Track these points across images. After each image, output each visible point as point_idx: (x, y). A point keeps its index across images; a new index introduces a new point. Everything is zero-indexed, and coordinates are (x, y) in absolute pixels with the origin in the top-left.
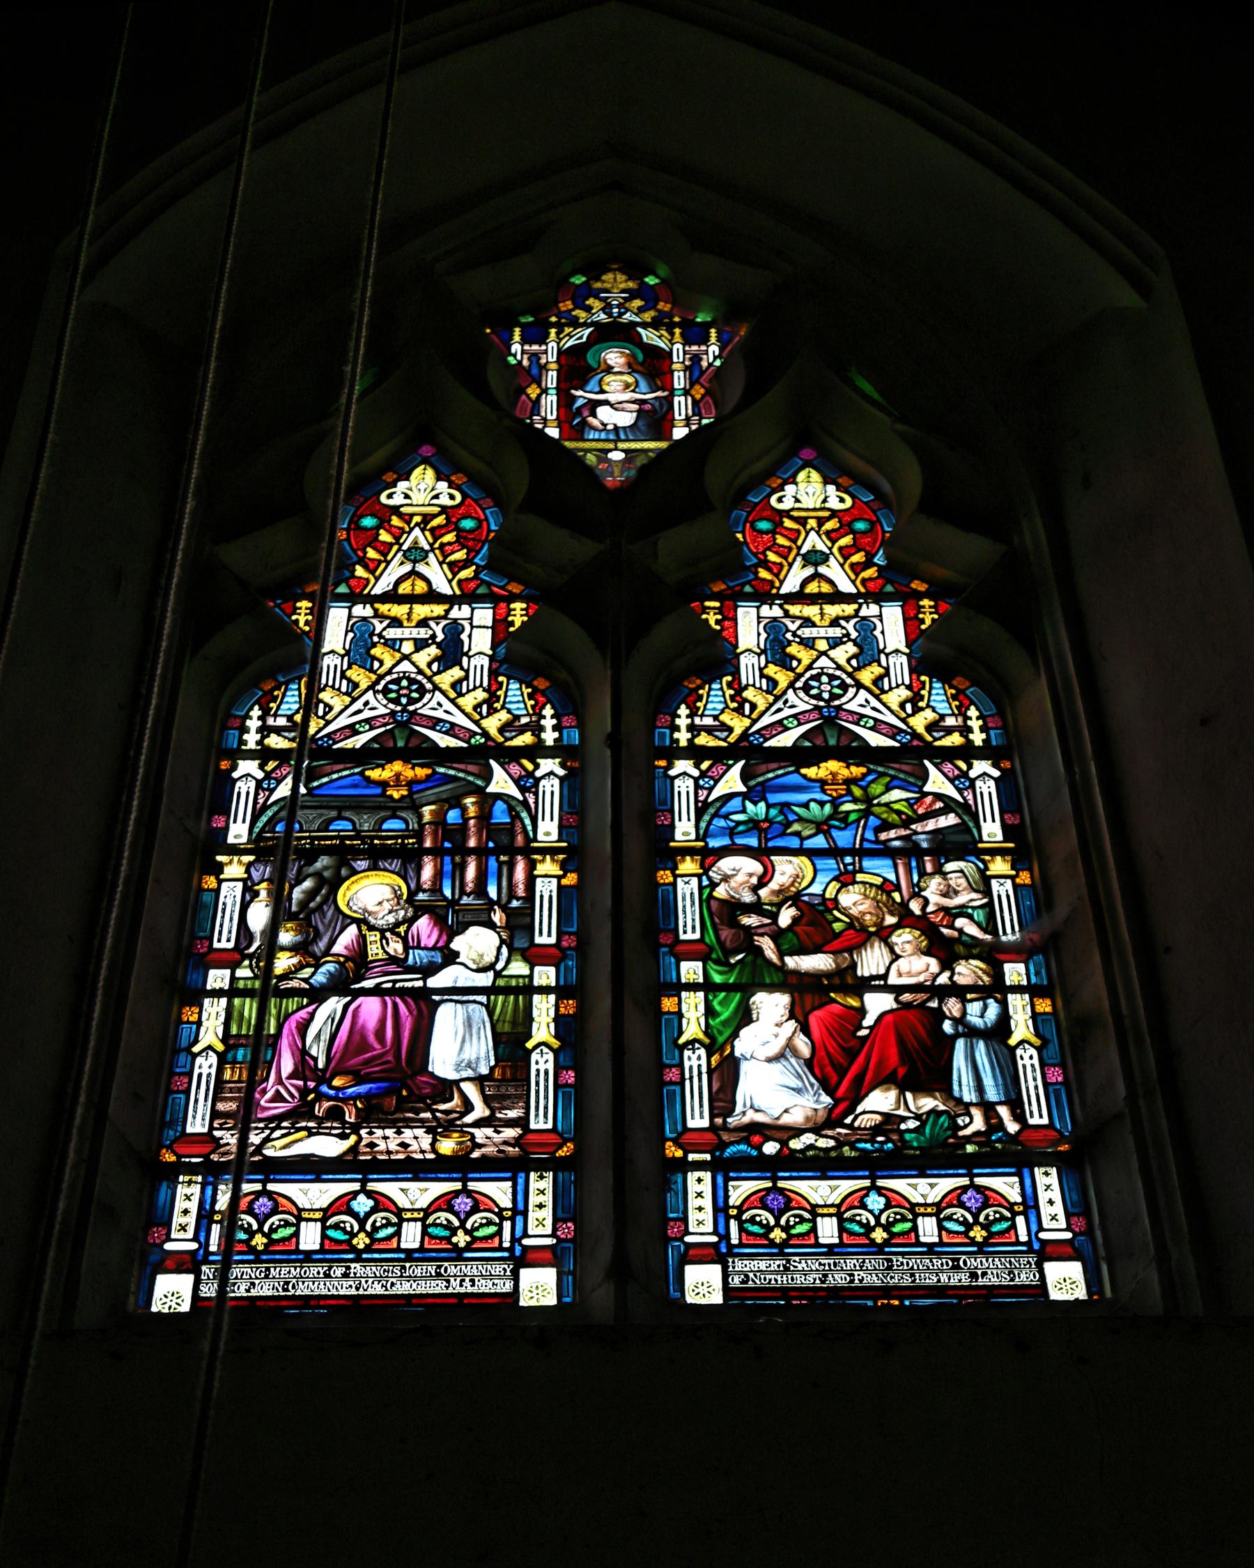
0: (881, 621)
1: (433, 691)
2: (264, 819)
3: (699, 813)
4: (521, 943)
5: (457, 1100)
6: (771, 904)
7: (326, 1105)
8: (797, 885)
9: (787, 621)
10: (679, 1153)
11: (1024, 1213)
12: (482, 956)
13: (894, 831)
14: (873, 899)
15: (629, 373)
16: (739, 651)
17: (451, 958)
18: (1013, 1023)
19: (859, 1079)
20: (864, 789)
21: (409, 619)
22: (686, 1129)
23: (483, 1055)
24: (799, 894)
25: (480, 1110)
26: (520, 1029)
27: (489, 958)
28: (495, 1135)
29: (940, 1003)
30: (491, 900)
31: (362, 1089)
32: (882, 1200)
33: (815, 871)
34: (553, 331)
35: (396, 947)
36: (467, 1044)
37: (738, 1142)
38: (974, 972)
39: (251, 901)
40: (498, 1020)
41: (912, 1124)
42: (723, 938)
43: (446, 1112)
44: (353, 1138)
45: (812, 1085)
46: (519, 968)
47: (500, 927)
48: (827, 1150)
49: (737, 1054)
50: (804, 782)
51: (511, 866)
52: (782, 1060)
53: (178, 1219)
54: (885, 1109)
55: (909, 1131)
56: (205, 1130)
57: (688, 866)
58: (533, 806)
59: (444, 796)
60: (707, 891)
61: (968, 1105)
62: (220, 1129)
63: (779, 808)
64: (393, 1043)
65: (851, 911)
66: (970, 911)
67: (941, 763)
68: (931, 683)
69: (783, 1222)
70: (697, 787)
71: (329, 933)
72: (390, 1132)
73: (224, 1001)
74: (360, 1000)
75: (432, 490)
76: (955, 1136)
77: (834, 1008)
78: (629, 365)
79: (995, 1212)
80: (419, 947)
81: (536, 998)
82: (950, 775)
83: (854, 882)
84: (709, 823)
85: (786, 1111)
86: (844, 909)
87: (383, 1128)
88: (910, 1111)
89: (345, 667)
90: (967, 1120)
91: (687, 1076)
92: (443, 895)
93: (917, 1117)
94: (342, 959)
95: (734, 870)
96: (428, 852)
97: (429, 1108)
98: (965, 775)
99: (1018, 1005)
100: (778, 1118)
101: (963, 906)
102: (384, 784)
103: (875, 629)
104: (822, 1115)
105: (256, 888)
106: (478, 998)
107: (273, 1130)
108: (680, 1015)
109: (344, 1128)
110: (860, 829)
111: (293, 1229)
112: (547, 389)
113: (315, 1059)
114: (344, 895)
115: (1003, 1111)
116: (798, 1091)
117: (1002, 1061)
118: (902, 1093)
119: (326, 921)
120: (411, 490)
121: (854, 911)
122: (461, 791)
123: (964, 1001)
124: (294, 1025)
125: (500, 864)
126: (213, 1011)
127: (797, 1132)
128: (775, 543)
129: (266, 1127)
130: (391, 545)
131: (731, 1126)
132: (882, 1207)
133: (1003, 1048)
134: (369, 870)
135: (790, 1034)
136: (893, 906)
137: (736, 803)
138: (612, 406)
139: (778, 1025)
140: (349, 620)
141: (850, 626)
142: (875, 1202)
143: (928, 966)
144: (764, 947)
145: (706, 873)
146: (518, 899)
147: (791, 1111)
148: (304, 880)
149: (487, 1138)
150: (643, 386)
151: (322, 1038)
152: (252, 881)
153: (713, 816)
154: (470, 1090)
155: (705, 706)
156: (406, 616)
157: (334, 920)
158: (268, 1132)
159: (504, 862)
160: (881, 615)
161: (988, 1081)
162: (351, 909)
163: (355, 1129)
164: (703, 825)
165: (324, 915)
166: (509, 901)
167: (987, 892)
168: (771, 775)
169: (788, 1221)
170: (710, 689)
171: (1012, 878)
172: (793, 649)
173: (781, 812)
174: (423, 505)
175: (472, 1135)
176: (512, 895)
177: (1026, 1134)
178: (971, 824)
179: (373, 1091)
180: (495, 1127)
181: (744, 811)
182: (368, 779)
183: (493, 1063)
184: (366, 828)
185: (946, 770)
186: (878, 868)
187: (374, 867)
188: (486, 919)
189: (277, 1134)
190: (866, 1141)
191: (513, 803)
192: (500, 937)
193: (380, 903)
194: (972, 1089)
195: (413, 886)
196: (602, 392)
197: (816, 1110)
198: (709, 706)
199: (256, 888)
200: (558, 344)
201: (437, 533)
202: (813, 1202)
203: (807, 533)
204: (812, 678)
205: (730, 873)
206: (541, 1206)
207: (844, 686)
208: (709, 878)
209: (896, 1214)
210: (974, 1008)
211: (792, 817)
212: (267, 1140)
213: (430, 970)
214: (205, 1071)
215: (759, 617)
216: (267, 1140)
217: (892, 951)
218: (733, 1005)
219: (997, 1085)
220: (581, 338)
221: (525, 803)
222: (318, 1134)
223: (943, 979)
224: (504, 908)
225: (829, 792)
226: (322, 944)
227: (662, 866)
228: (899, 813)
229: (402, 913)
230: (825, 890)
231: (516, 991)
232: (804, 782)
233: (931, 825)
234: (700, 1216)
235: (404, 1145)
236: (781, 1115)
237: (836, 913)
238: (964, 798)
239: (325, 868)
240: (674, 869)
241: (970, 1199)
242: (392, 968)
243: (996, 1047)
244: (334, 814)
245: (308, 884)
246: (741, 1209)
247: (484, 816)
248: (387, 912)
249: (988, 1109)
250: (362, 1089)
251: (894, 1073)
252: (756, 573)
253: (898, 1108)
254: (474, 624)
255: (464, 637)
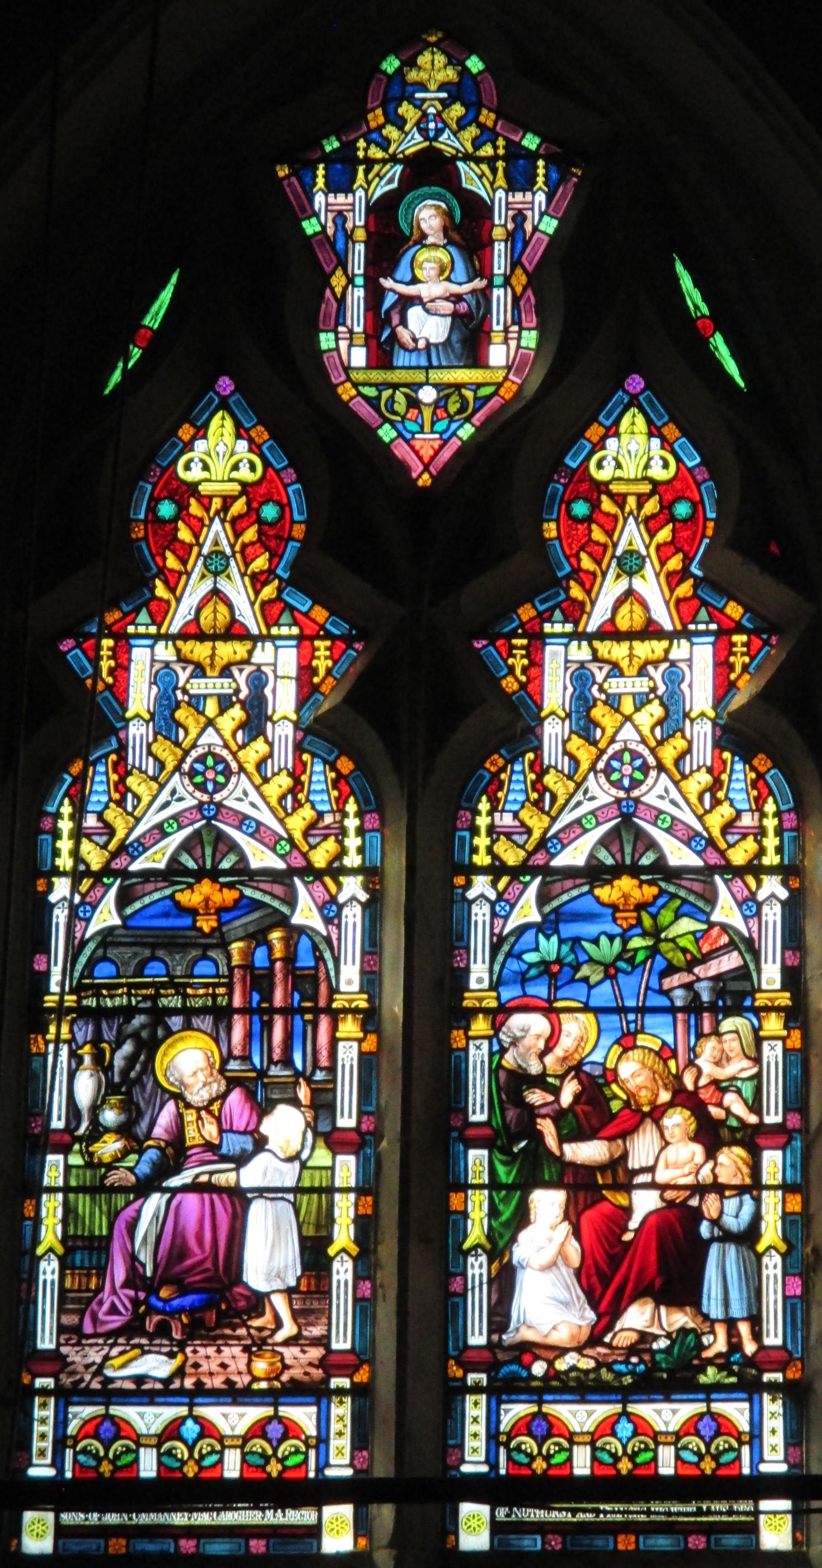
0: (690, 667)
1: (239, 773)
2: (83, 960)
3: (495, 949)
4: (325, 1127)
5: (268, 1315)
6: (555, 1076)
7: (156, 1318)
8: (580, 1050)
9: (593, 667)
10: (459, 1373)
11: (750, 1443)
12: (288, 1142)
13: (676, 976)
14: (651, 1069)
15: (444, 247)
16: (543, 714)
17: (260, 1144)
18: (763, 1225)
19: (621, 1289)
20: (654, 917)
21: (212, 665)
22: (467, 1347)
23: (290, 1263)
24: (581, 1063)
25: (289, 1329)
26: (323, 1233)
27: (295, 1146)
28: (300, 1355)
29: (701, 1200)
30: (296, 1069)
31: (189, 1300)
32: (630, 1427)
33: (599, 1031)
34: (361, 169)
35: (211, 1130)
36: (276, 1253)
37: (510, 1362)
38: (735, 1163)
39: (77, 1069)
40: (303, 1222)
41: (663, 1343)
42: (508, 1119)
43: (260, 1329)
44: (180, 1358)
45: (578, 1298)
46: (322, 1157)
47: (305, 1106)
48: (587, 1372)
49: (515, 1261)
50: (597, 908)
51: (315, 1025)
52: (554, 1268)
53: (36, 1444)
54: (639, 1327)
55: (660, 1351)
56: (53, 1346)
57: (480, 1026)
58: (335, 943)
59: (251, 929)
60: (496, 1058)
61: (713, 1322)
62: (66, 1344)
63: (570, 943)
64: (211, 1247)
65: (628, 1085)
66: (739, 1083)
67: (731, 880)
68: (733, 763)
69: (544, 1451)
70: (494, 915)
71: (150, 1112)
72: (211, 1351)
73: (60, 1196)
74: (179, 1197)
75: (232, 455)
76: (698, 1357)
77: (603, 1207)
78: (445, 230)
79: (725, 1442)
80: (231, 1131)
81: (337, 1197)
82: (739, 896)
83: (634, 1047)
84: (503, 966)
85: (554, 1328)
86: (623, 1081)
87: (205, 1346)
88: (663, 1329)
89: (151, 739)
90: (711, 1338)
91: (470, 1286)
92: (252, 1064)
93: (668, 1336)
94: (163, 1144)
95: (523, 1030)
96: (239, 1011)
97: (244, 1324)
98: (753, 895)
99: (772, 1202)
100: (546, 1336)
101: (734, 1078)
102: (193, 912)
103: (683, 680)
104: (585, 1335)
105: (80, 1052)
106: (286, 1196)
107: (112, 1346)
108: (465, 1214)
109: (171, 1345)
110: (646, 973)
111: (133, 1456)
112: (354, 275)
113: (144, 1266)
114: (162, 1063)
115: (744, 1329)
116: (566, 1304)
117: (749, 1270)
118: (657, 1307)
119: (146, 1096)
120: (210, 456)
121: (631, 1085)
122: (267, 922)
123: (722, 1197)
124: (123, 1226)
125: (305, 1023)
126: (51, 1205)
127: (562, 1351)
128: (590, 540)
129: (105, 1344)
130: (191, 546)
131: (506, 1344)
132: (629, 1434)
133: (752, 1254)
134: (184, 1029)
135: (562, 1239)
136: (668, 1077)
137: (529, 936)
138: (423, 305)
139: (554, 1228)
140: (152, 666)
141: (657, 674)
142: (625, 1429)
143: (694, 1154)
144: (546, 1132)
145: (496, 1035)
146: (322, 1069)
147: (559, 1328)
148: (124, 1042)
149: (295, 1358)
150: (460, 272)
151: (149, 1240)
152: (77, 1043)
153: (509, 955)
154: (280, 1303)
155: (506, 796)
156: (208, 661)
157: (153, 1094)
158: (107, 1349)
159: (309, 1021)
160: (690, 660)
161: (734, 1295)
162: (168, 1080)
163: (182, 1345)
164: (497, 968)
165: (143, 1087)
166: (313, 1073)
167: (757, 1060)
168: (565, 898)
169: (549, 1450)
170: (512, 772)
171: (784, 1039)
172: (598, 713)
173: (572, 950)
174: (223, 481)
175: (281, 1354)
176: (316, 1066)
177: (761, 1354)
178: (752, 966)
179: (197, 1304)
180: (302, 1345)
181: (537, 949)
182: (177, 904)
183: (299, 1273)
184: (179, 973)
185: (735, 890)
186: (658, 1027)
187: (188, 1026)
188: (292, 1095)
189: (115, 1351)
190: (621, 1363)
191: (317, 939)
192: (305, 1118)
193: (195, 1073)
194: (719, 1303)
195: (225, 1051)
196: (415, 281)
197: (580, 1327)
198: (511, 797)
199: (80, 1052)
200: (366, 191)
201: (239, 526)
202: (571, 1429)
203: (625, 520)
204: (614, 757)
205: (519, 1034)
206: (340, 1434)
207: (645, 769)
208: (500, 1042)
209: (641, 1442)
210: (731, 1205)
211: (583, 957)
212: (106, 1358)
213: (241, 1160)
214: (49, 1277)
215: (567, 661)
216: (106, 1358)
217: (662, 1136)
218: (514, 1203)
219: (741, 1299)
220: (391, 181)
221: (328, 940)
222: (150, 1352)
223: (705, 1175)
224: (309, 1081)
225: (619, 922)
226: (144, 1124)
227: (455, 1024)
228: (684, 951)
229: (215, 1086)
230: (606, 1058)
231: (319, 1190)
232: (597, 908)
233: (714, 968)
234: (475, 1444)
235: (224, 1366)
236: (549, 1333)
237: (614, 1087)
238: (749, 929)
239: (143, 1027)
240: (467, 1028)
241: (705, 1427)
242: (209, 1156)
243: (746, 1254)
244: (147, 953)
245: (128, 1048)
246: (510, 1435)
247: (290, 959)
248: (201, 1085)
249: (731, 1324)
250: (189, 1300)
251: (652, 1282)
252: (567, 589)
253: (652, 1325)
254: (279, 673)
255: (268, 691)
